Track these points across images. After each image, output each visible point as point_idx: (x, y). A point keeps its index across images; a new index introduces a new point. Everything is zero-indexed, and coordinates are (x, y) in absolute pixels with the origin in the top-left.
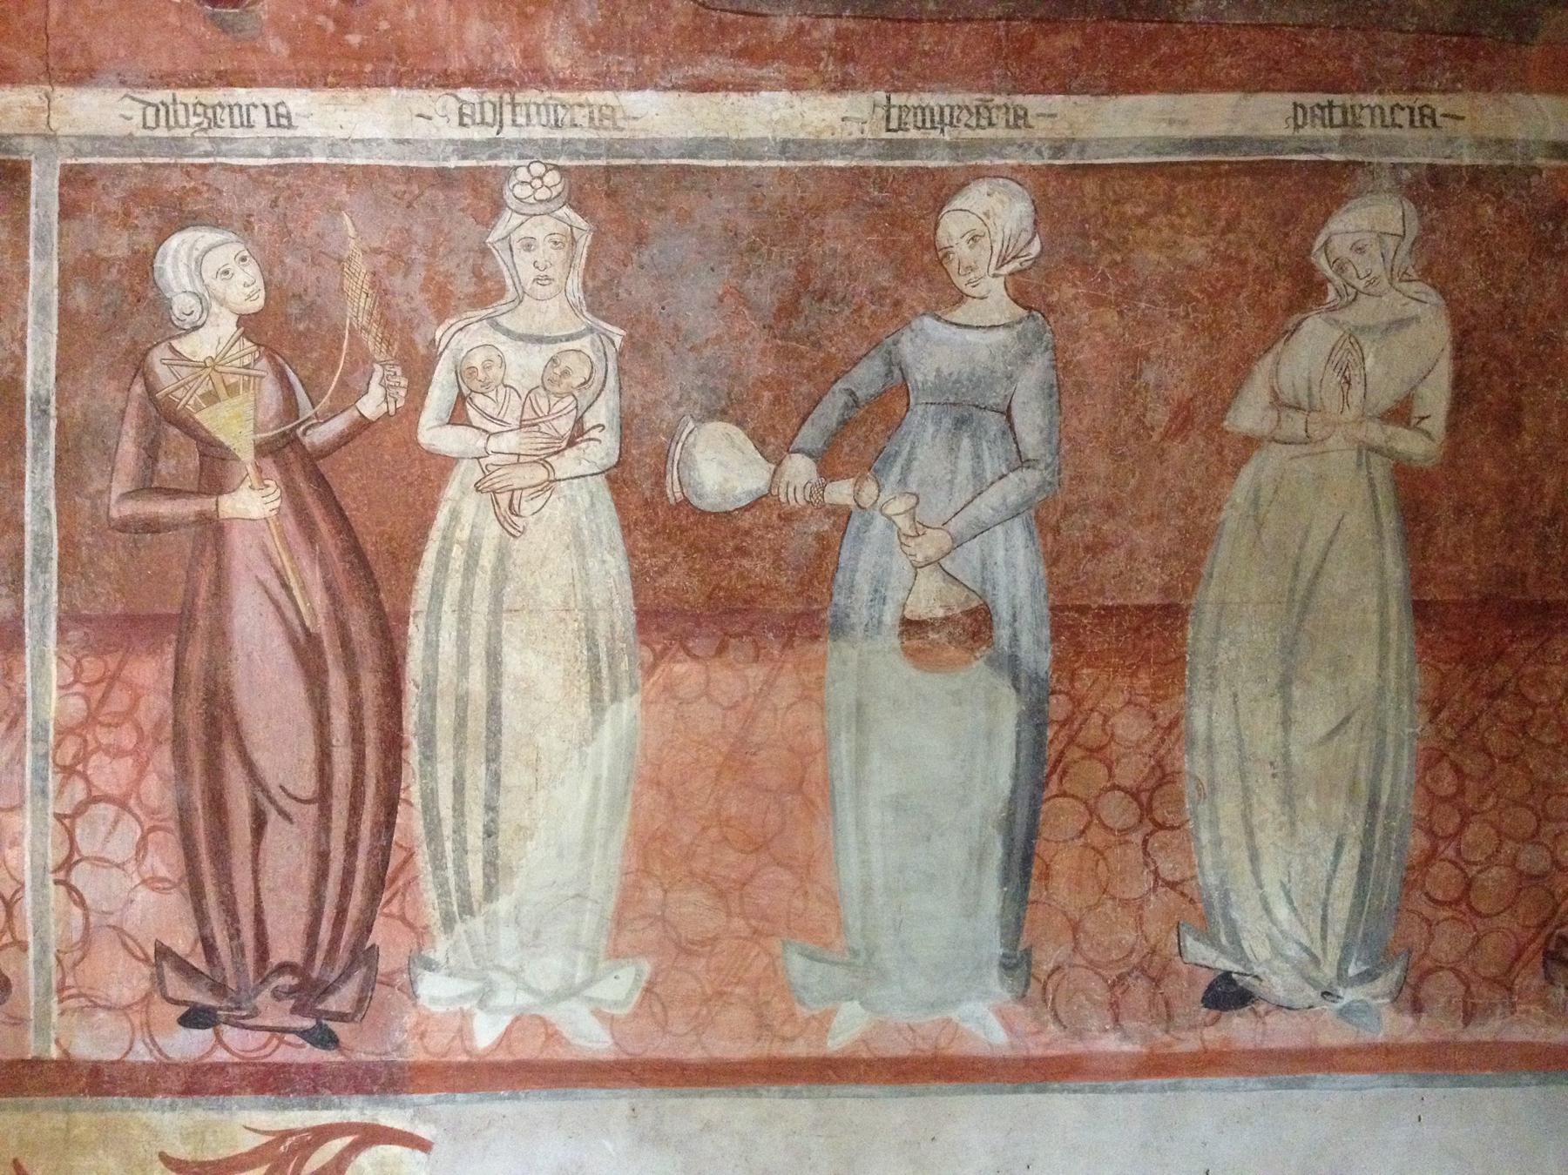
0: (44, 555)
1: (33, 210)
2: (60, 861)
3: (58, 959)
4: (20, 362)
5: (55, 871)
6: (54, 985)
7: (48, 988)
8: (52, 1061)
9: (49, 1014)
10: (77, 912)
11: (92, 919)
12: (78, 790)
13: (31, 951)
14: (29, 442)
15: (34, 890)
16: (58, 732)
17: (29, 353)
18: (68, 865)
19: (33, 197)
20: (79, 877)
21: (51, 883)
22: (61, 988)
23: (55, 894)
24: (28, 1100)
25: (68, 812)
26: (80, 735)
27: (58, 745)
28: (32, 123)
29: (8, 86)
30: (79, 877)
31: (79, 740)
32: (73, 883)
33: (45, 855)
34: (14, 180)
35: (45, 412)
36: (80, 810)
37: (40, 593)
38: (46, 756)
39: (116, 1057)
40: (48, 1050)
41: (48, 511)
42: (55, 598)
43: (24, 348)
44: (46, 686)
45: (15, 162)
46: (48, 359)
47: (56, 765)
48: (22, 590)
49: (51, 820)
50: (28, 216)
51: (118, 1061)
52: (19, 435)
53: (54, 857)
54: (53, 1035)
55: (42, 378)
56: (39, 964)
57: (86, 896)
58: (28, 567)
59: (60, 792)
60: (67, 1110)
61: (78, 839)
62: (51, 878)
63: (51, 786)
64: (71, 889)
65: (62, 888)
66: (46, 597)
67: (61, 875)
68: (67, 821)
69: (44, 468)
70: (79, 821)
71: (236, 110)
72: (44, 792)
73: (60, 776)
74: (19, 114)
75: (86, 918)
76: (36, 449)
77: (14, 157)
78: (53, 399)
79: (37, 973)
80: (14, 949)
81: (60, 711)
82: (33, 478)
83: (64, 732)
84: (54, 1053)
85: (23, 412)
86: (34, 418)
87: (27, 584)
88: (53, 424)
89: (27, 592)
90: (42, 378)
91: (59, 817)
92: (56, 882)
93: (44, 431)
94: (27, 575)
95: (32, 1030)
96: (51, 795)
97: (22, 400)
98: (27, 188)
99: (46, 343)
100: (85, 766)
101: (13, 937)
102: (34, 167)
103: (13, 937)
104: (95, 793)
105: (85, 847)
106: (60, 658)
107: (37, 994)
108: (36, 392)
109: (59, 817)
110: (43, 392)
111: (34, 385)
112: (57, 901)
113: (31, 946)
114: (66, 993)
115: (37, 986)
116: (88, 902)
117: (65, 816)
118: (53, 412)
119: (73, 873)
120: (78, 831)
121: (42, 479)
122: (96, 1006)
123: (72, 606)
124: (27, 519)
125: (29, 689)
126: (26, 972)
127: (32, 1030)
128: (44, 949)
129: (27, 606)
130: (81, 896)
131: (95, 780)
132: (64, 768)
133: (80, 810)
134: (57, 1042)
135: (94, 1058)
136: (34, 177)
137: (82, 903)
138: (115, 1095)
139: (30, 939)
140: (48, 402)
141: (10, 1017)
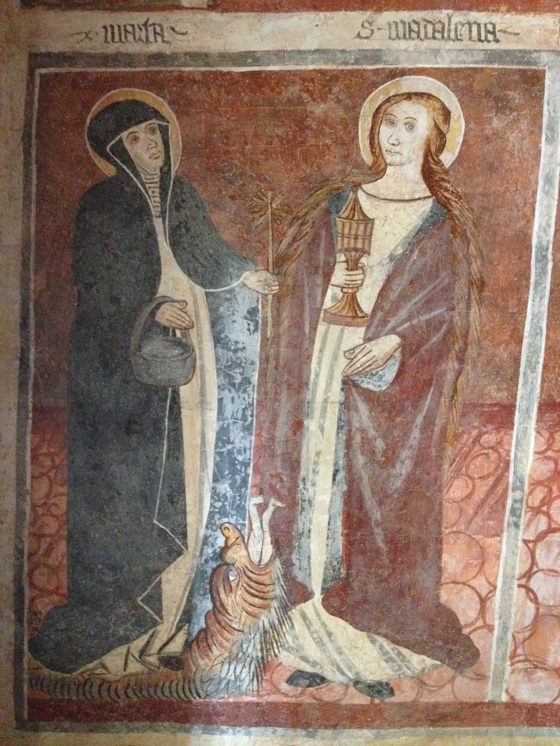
0: (534, 360)
1: (545, 107)
2: (524, 572)
3: (514, 637)
4: (529, 221)
5: (519, 579)
6: (508, 655)
7: (504, 655)
8: (503, 703)
9: (503, 673)
10: (531, 606)
11: (541, 610)
12: (542, 523)
13: (496, 632)
14: (532, 280)
15: (503, 592)
16: (531, 484)
17: (537, 214)
18: (528, 575)
19: (546, 97)
20: (535, 583)
21: (515, 587)
22: (513, 655)
23: (518, 594)
24: (484, 729)
25: (532, 538)
26: (547, 486)
27: (530, 493)
28: (547, 42)
29: (532, 14)
30: (535, 583)
31: (546, 490)
32: (531, 587)
33: (514, 568)
34: (533, 85)
35: (545, 257)
36: (541, 537)
37: (529, 387)
38: (521, 501)
39: (547, 701)
40: (500, 696)
41: (541, 328)
42: (538, 391)
43: (534, 210)
44: (525, 452)
45: (535, 71)
46: (550, 217)
47: (528, 506)
48: (517, 385)
49: (520, 544)
50: (541, 112)
51: (549, 705)
52: (525, 275)
53: (520, 568)
54: (505, 686)
55: (545, 231)
56: (501, 640)
57: (539, 595)
58: (522, 369)
59: (528, 525)
60: (511, 735)
61: (537, 557)
62: (516, 582)
63: (523, 521)
64: (529, 590)
65: (523, 590)
66: (532, 390)
67: (523, 581)
68: (531, 545)
69: (541, 298)
70: (540, 546)
71: (475, 28)
72: (517, 525)
73: (529, 514)
74: (537, 34)
75: (537, 609)
76: (537, 284)
77: (533, 67)
78: (551, 247)
79: (498, 647)
80: (485, 630)
81: (534, 470)
82: (533, 306)
83: (535, 484)
84: (504, 698)
85: (530, 257)
86: (537, 260)
87: (521, 380)
88: (550, 266)
89: (520, 386)
90: (545, 231)
91: (526, 542)
92: (520, 586)
93: (543, 271)
94: (521, 374)
95: (490, 684)
96: (522, 527)
97: (529, 248)
98: (542, 91)
99: (549, 206)
100: (549, 508)
101: (485, 623)
102: (547, 75)
103: (485, 623)
104: (554, 526)
105: (543, 561)
106: (538, 432)
107: (496, 659)
108: (540, 243)
109: (526, 542)
110: (545, 243)
111: (539, 237)
112: (517, 599)
113: (496, 628)
114: (516, 659)
115: (497, 654)
116: (540, 600)
117: (529, 541)
118: (550, 257)
119: (532, 580)
120: (538, 552)
121: (540, 306)
122: (536, 667)
123: (550, 396)
124: (526, 334)
125: (512, 454)
126: (491, 646)
127: (490, 684)
128: (505, 629)
129: (519, 397)
130: (535, 594)
131: (555, 517)
132: (532, 508)
133: (541, 537)
134: (507, 691)
135: (532, 701)
136: (547, 82)
137: (535, 600)
138: (544, 725)
139: (496, 623)
140: (547, 249)
141: (477, 675)
